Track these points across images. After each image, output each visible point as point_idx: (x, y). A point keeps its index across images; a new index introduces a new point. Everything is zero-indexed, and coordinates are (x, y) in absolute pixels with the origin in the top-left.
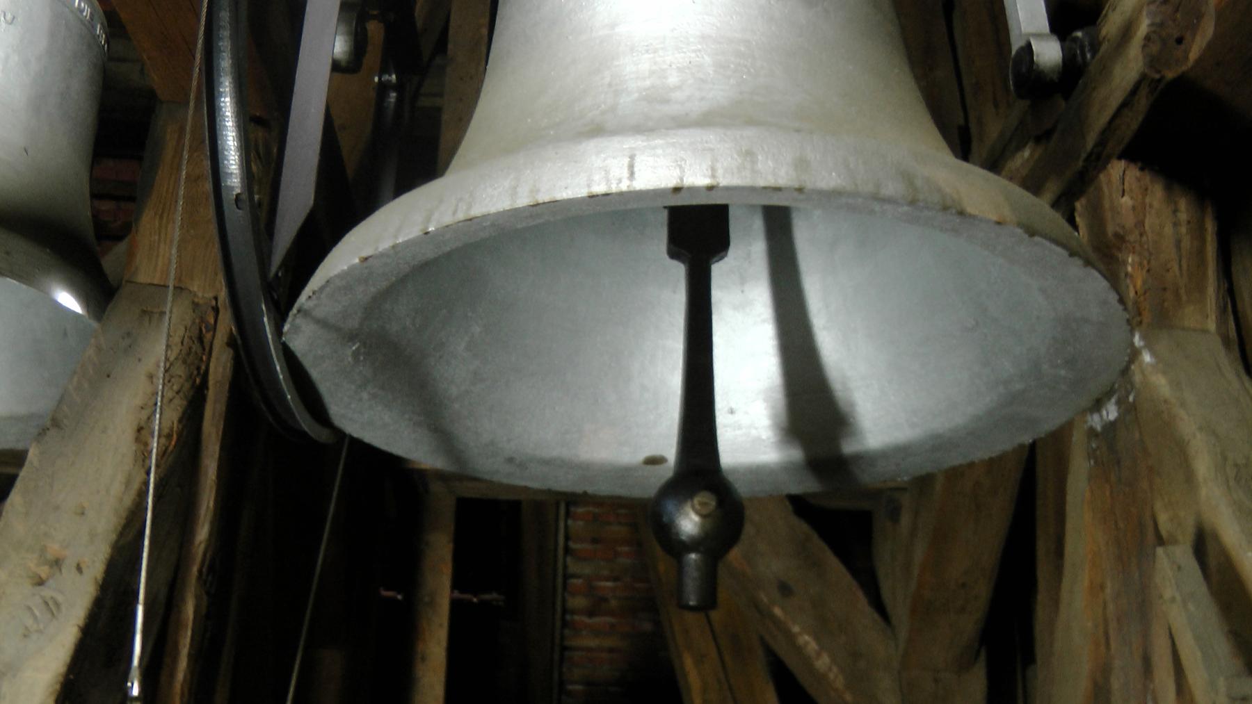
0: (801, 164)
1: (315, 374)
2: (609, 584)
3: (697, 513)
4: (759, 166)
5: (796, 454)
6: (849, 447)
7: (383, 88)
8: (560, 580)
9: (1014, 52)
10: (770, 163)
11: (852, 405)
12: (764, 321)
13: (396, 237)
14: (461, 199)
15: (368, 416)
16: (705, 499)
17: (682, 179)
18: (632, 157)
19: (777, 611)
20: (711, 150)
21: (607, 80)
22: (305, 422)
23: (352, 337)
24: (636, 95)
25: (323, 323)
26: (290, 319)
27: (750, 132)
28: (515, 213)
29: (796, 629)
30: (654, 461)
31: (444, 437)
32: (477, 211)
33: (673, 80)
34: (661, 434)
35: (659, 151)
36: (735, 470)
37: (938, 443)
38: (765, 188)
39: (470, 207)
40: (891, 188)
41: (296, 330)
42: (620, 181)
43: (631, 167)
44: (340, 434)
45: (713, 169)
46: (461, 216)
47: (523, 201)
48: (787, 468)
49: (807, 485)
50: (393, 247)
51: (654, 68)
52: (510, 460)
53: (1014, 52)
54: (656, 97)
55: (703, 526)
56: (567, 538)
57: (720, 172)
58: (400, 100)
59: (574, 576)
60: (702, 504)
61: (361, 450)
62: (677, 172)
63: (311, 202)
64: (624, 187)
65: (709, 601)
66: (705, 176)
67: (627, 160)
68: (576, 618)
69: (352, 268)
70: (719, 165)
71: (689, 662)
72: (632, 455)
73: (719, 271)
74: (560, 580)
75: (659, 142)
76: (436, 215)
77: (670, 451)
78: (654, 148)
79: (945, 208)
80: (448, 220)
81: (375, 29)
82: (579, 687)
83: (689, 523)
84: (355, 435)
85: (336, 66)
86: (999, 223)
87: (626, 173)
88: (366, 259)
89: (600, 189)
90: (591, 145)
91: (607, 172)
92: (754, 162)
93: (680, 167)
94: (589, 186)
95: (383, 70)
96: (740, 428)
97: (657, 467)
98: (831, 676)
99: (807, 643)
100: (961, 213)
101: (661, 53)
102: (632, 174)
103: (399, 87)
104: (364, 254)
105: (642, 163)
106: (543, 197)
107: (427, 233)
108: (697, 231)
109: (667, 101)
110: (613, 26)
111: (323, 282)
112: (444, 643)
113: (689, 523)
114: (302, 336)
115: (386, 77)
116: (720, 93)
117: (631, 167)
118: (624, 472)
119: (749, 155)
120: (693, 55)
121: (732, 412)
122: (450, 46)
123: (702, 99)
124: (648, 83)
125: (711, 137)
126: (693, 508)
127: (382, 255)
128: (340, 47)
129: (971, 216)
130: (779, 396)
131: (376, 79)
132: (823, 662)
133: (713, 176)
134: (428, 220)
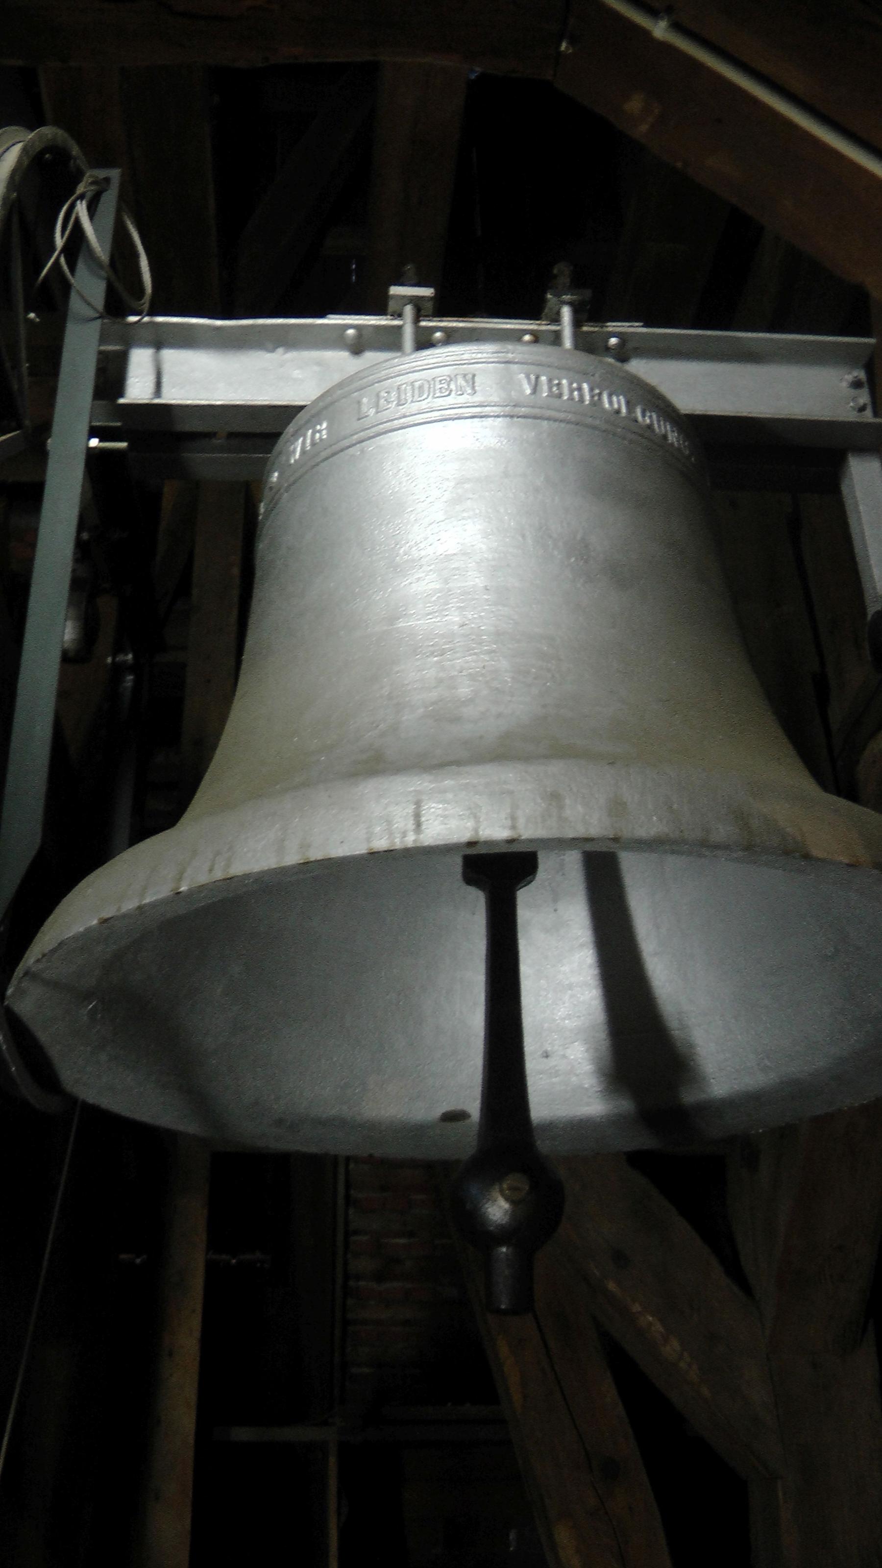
0: (616, 807)
1: (43, 1037)
2: (402, 1241)
3: (507, 1199)
4: (568, 812)
5: (626, 1105)
6: (689, 1097)
7: (118, 670)
8: (340, 1237)
9: (869, 617)
10: (580, 808)
11: (691, 1046)
12: (582, 946)
13: (142, 895)
14: (218, 853)
15: (106, 1081)
16: (518, 1181)
17: (476, 831)
18: (418, 804)
19: (611, 1286)
20: (511, 793)
21: (385, 691)
22: (28, 1090)
23: (88, 996)
24: (421, 711)
25: (54, 985)
26: (14, 981)
27: (556, 767)
28: (283, 871)
29: (636, 1308)
30: (454, 1117)
31: (199, 1099)
32: (238, 869)
33: (464, 690)
34: (461, 1085)
35: (450, 796)
36: (549, 1127)
37: (794, 1090)
38: (573, 839)
39: (228, 866)
40: (722, 831)
41: (21, 992)
42: (404, 834)
43: (417, 816)
44: (72, 1101)
45: (513, 818)
46: (219, 875)
47: (292, 858)
48: (615, 1122)
49: (644, 1141)
50: (140, 908)
51: (441, 675)
52: (280, 1122)
53: (869, 617)
54: (443, 714)
55: (513, 1214)
56: (348, 1186)
57: (521, 822)
58: (137, 683)
59: (356, 1232)
60: (512, 1189)
61: (98, 1119)
62: (470, 824)
63: (38, 840)
64: (410, 840)
65: (524, 1302)
66: (504, 827)
67: (411, 808)
68: (362, 1283)
69: (88, 930)
70: (519, 813)
71: (504, 1350)
72: (426, 1110)
73: (524, 897)
74: (340, 1237)
75: (449, 783)
76: (189, 871)
77: (474, 1107)
78: (445, 791)
79: (787, 853)
80: (203, 878)
81: (108, 606)
82: (366, 1370)
83: (498, 1210)
84: (91, 1101)
85: (67, 658)
86: (849, 865)
87: (411, 825)
88: (106, 921)
89: (381, 844)
90: (369, 787)
91: (389, 823)
92: (561, 807)
93: (476, 817)
94: (368, 840)
95: (118, 649)
96: (557, 1074)
97: (460, 1123)
98: (682, 1365)
99: (650, 1324)
100: (807, 857)
101: (448, 655)
102: (418, 825)
103: (134, 668)
104: (106, 914)
105: (432, 810)
106: (315, 854)
107: (179, 893)
108: (499, 874)
109: (456, 719)
110: (392, 619)
111: (55, 944)
112: (197, 1334)
113: (498, 1210)
114: (27, 1000)
115: (120, 658)
116: (520, 707)
117: (417, 816)
118: (418, 1131)
119: (555, 798)
120: (487, 658)
121: (546, 1055)
122: (195, 592)
123: (499, 716)
124: (434, 695)
125: (508, 775)
126: (503, 1195)
127: (124, 916)
128: (69, 633)
129: (818, 859)
130: (602, 1035)
131: (109, 660)
132: (672, 1348)
133: (513, 827)
134: (179, 879)
